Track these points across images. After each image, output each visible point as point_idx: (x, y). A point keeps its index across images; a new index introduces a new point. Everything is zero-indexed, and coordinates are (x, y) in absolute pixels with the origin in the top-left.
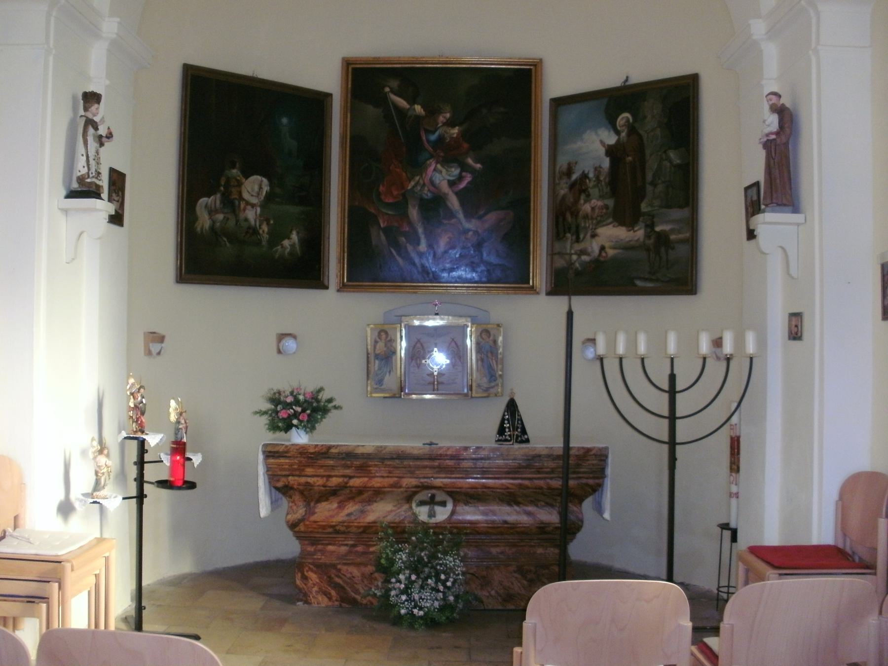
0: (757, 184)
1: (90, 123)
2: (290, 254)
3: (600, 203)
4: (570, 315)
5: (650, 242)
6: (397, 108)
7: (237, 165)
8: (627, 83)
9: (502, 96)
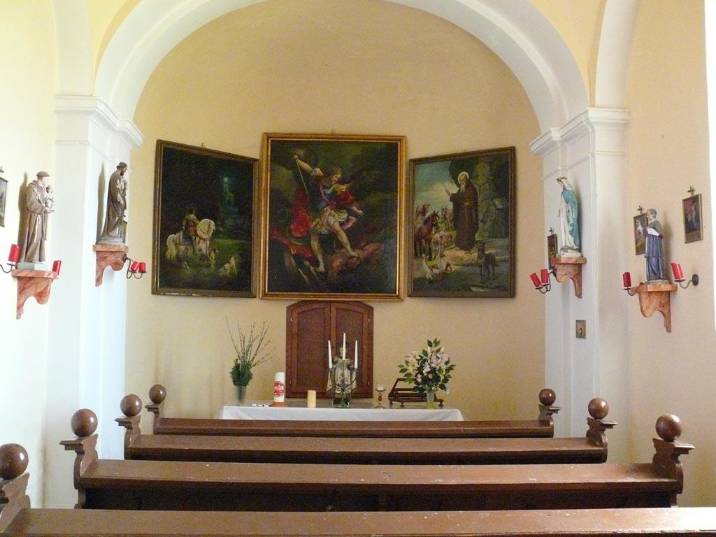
2: (231, 273)
6: (302, 169)
7: (194, 212)
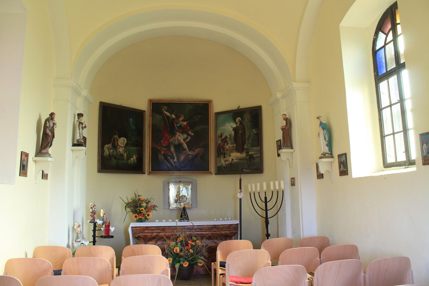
0: (280, 140)
1: (81, 123)
2: (133, 162)
3: (231, 146)
4: (240, 180)
5: (248, 157)
6: (166, 115)
8: (240, 108)
9: (199, 111)
